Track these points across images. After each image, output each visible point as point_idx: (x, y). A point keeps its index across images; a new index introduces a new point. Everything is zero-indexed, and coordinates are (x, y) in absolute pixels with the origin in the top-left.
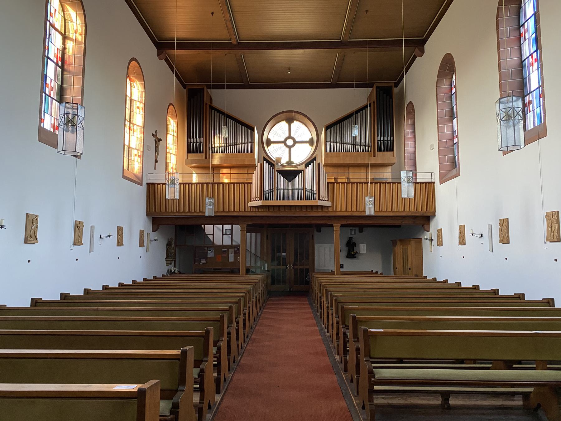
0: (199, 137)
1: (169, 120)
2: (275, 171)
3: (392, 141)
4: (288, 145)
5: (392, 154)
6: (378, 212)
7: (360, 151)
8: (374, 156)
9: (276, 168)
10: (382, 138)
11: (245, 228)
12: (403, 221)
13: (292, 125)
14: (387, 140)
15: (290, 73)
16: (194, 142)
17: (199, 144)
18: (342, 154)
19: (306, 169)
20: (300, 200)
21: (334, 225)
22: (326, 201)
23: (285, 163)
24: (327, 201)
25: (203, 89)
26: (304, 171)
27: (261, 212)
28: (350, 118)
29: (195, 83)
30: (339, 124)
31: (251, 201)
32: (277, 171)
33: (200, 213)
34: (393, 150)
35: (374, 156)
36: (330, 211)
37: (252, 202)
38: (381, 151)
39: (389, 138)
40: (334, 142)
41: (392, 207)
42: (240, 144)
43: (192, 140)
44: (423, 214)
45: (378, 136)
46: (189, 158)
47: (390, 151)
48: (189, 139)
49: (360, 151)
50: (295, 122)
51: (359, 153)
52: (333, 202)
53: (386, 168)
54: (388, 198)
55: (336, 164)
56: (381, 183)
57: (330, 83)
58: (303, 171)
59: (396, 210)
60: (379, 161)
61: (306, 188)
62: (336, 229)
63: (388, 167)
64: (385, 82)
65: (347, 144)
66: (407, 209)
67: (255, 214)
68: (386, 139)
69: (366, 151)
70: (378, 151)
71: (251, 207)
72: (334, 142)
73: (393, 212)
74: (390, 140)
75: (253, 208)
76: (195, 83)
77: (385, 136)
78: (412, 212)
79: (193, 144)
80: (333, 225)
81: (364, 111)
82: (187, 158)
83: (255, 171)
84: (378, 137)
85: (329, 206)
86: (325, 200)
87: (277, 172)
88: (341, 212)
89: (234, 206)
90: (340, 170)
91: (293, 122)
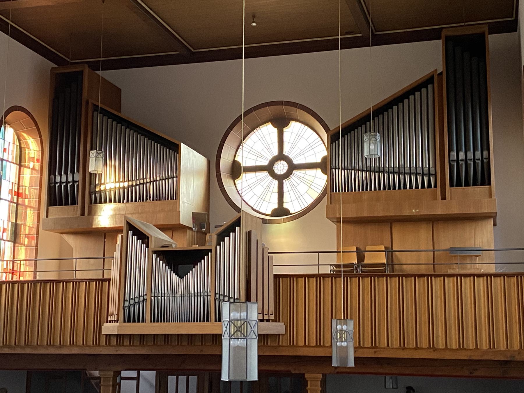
0: (71, 172)
1: (25, 139)
2: (151, 253)
3: (485, 161)
4: (287, 171)
5: (487, 192)
6: (396, 348)
7: (411, 187)
8: (444, 198)
9: (153, 245)
10: (462, 155)
11: (111, 379)
12: (474, 370)
13: (287, 131)
14: (466, 160)
15: (254, 24)
16: (61, 183)
17: (64, 186)
18: (366, 195)
19: (218, 247)
20: (197, 321)
21: (307, 375)
22: (271, 323)
23: (269, 213)
24: (273, 321)
25: (81, 73)
26: (213, 251)
27: (127, 346)
28: (385, 113)
29: (463, 24)
30: (360, 128)
31: (107, 322)
32: (155, 252)
33: (6, 349)
34: (489, 184)
35: (444, 198)
36: (282, 346)
37: (108, 324)
38: (459, 184)
39: (478, 154)
40: (350, 168)
41: (431, 334)
42: (160, 180)
43: (58, 179)
44: (514, 357)
45: (450, 150)
46: (50, 217)
47: (483, 184)
48: (52, 176)
49: (411, 187)
50: (293, 124)
51: (426, 190)
52: (290, 326)
53: (480, 223)
54: (396, 319)
55: (352, 218)
56: (403, 276)
57: (510, 19)
58: (210, 251)
59: (441, 345)
60: (455, 210)
61: (217, 291)
62: (311, 386)
63: (489, 220)
64: (466, 24)
65: (379, 172)
66: (470, 344)
67: (117, 351)
68: (470, 155)
69: (430, 186)
70: (452, 185)
71: (107, 335)
72: (350, 168)
73: (435, 349)
74: (466, 160)
75: (112, 338)
76: (463, 24)
77: (469, 150)
78: (485, 352)
79: (60, 187)
80: (304, 374)
81: (417, 94)
82: (47, 217)
83: (115, 253)
84: (452, 153)
85: (279, 335)
86: (268, 321)
87: (155, 256)
88: (308, 349)
89: (72, 335)
90: (370, 231)
91: (286, 125)
